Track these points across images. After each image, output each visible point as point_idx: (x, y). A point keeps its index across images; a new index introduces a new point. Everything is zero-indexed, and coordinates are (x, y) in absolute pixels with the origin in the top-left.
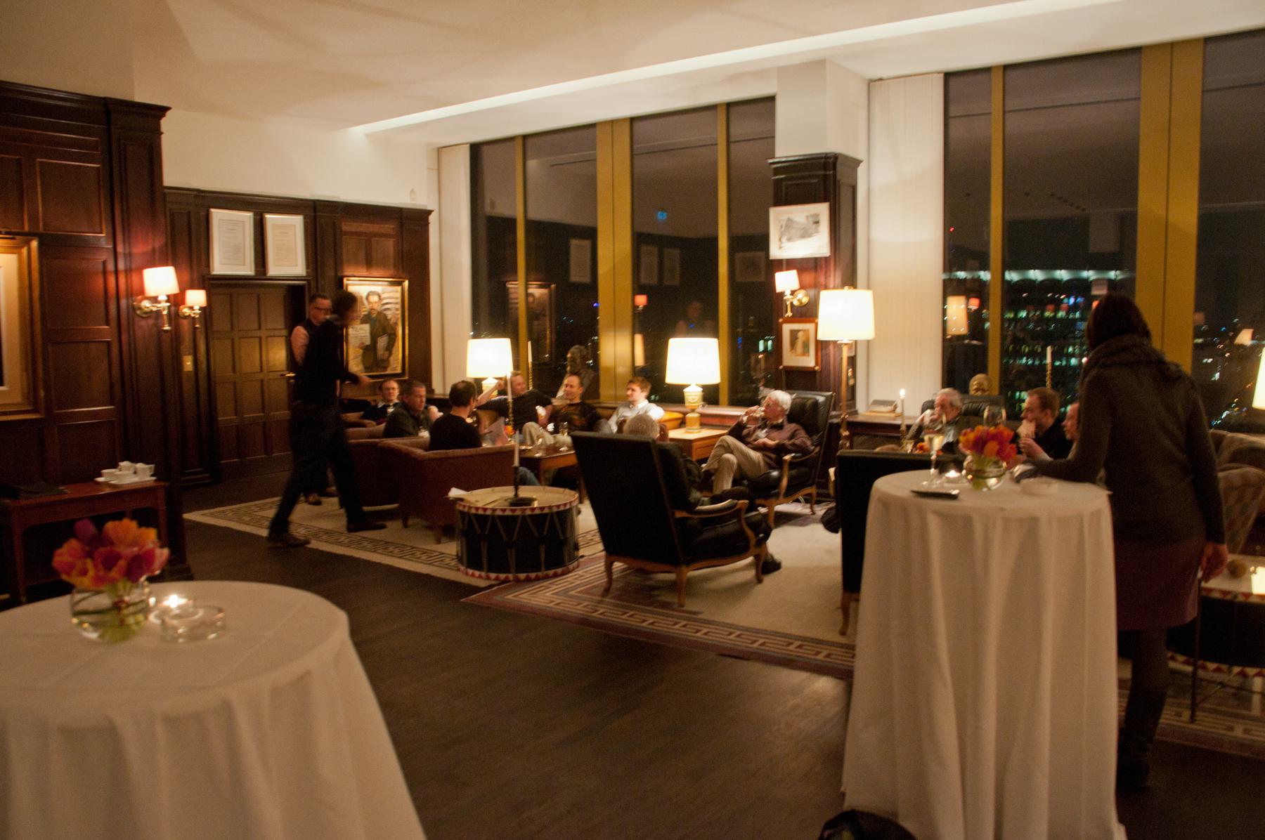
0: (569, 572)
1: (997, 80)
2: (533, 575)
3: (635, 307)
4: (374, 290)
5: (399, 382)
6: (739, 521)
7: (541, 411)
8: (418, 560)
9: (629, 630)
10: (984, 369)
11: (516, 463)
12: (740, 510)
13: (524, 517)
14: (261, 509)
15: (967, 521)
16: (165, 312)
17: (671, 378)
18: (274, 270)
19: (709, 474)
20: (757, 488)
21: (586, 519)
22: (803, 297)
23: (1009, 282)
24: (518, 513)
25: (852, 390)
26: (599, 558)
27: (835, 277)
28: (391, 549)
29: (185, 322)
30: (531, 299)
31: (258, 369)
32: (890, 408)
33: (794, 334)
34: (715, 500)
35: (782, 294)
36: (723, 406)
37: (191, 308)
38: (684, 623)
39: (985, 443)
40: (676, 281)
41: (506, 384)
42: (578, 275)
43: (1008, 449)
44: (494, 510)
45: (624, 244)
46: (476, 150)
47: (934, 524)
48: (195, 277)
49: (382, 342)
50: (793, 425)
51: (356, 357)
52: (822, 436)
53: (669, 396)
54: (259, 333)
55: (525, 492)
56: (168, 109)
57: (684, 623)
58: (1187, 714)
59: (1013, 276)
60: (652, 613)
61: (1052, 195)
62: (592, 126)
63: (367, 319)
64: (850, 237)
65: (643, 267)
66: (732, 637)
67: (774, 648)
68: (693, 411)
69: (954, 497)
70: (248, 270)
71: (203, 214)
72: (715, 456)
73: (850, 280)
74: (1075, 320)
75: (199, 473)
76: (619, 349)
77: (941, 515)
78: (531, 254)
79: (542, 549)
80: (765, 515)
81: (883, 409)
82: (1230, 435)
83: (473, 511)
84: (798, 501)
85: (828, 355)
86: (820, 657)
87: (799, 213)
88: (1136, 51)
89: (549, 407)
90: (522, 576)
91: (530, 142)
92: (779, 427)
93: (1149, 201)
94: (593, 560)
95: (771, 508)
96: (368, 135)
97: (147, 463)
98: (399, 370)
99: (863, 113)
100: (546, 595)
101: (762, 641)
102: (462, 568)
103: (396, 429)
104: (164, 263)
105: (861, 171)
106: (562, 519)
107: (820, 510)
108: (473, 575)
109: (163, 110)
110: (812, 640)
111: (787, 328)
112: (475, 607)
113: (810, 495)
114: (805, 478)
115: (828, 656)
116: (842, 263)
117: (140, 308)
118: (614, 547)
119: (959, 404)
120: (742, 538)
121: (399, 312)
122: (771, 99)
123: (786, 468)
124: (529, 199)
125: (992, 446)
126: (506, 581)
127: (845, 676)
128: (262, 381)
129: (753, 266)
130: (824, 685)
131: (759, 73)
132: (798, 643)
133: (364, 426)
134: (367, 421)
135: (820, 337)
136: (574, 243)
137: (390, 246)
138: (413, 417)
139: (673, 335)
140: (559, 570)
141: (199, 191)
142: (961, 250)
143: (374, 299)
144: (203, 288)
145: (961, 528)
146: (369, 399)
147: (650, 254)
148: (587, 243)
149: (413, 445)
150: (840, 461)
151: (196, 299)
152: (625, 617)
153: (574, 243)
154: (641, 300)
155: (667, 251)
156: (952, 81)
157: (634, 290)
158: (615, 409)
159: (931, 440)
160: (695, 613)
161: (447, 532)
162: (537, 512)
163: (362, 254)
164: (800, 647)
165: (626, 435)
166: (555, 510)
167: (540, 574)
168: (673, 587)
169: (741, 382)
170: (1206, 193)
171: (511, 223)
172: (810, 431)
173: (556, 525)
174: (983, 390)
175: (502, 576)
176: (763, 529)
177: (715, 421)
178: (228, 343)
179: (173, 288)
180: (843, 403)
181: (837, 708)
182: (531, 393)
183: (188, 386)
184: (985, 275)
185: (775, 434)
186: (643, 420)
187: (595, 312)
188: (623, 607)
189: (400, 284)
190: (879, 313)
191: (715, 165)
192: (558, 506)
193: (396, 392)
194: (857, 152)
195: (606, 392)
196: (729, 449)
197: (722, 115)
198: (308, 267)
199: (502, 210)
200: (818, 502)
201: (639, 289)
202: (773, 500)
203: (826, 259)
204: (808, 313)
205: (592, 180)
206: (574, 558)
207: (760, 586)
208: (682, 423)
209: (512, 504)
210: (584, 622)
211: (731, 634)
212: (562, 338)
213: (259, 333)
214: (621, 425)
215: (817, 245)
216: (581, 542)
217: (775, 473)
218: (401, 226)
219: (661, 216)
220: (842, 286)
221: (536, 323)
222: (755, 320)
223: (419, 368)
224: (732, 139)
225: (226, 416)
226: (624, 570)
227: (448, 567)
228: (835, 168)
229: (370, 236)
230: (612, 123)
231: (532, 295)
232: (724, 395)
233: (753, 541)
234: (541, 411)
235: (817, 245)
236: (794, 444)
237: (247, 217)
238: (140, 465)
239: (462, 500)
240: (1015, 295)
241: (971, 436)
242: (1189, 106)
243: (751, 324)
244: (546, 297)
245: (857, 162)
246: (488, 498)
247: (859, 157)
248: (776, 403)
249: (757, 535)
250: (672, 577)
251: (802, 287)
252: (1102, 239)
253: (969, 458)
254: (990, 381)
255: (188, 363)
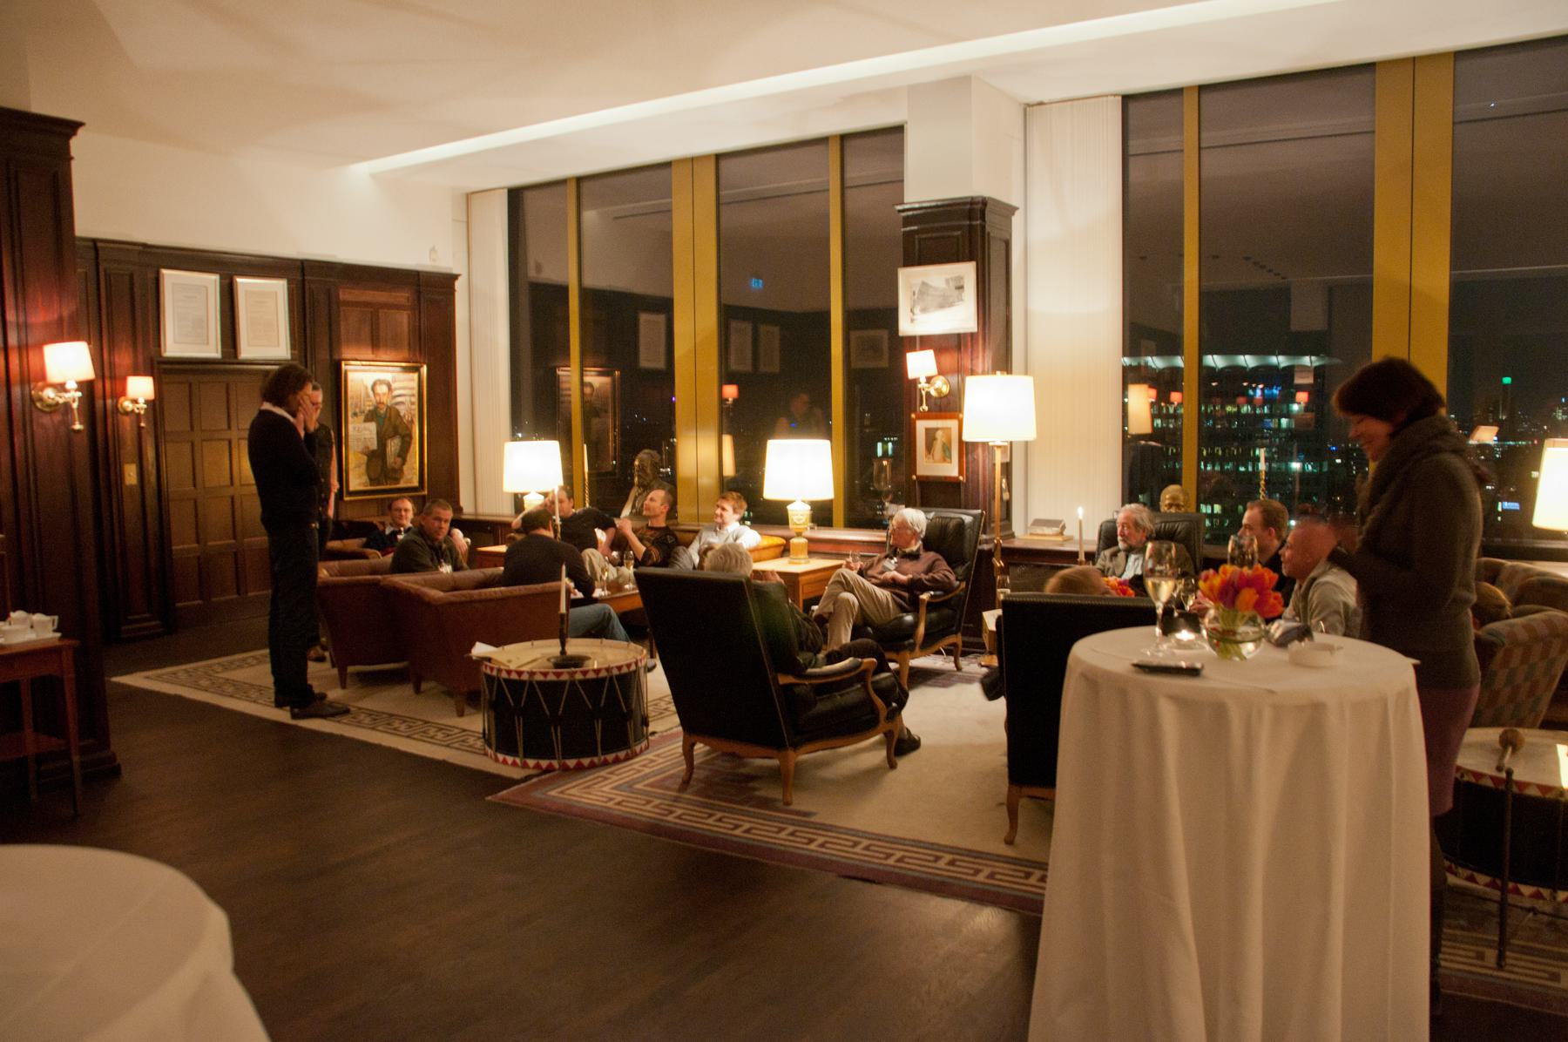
0: (635, 755)
1: (1190, 103)
2: (586, 761)
3: (722, 400)
4: (377, 379)
5: (413, 499)
6: (865, 687)
7: (601, 535)
8: (431, 740)
9: (715, 841)
10: (1175, 479)
11: (563, 609)
12: (865, 671)
13: (573, 683)
14: (226, 669)
15: (1219, 711)
16: (75, 405)
17: (771, 492)
18: (247, 351)
19: (822, 620)
20: (882, 637)
21: (657, 683)
22: (941, 386)
23: (1212, 369)
24: (565, 677)
25: (1007, 506)
26: (676, 735)
27: (984, 358)
28: (396, 724)
29: (127, 420)
30: (587, 390)
31: (228, 482)
32: (1056, 530)
33: (931, 434)
34: (833, 658)
35: (915, 382)
36: (838, 528)
37: (135, 401)
38: (791, 829)
39: (1237, 592)
40: (775, 368)
41: (553, 503)
42: (649, 359)
43: (1272, 600)
44: (532, 674)
45: (709, 319)
46: (516, 196)
47: (1169, 715)
48: (141, 358)
49: (393, 446)
50: (932, 554)
51: (358, 466)
52: (969, 569)
53: (768, 515)
54: (227, 435)
55: (576, 647)
56: (80, 124)
57: (791, 829)
58: (1491, 954)
59: (1215, 361)
60: (748, 814)
61: (1247, 259)
62: (667, 165)
63: (372, 416)
64: (1002, 308)
65: (732, 348)
66: (858, 849)
67: (917, 865)
68: (799, 535)
69: (1193, 672)
70: (212, 350)
71: (151, 276)
72: (829, 596)
73: (1004, 363)
74: (1263, 416)
75: (145, 620)
76: (702, 453)
77: (1180, 701)
78: (590, 332)
79: (599, 726)
80: (897, 673)
81: (1047, 531)
82: (1508, 563)
83: (504, 675)
84: (939, 653)
85: (975, 461)
86: (981, 878)
87: (937, 276)
88: (1369, 67)
89: (612, 530)
90: (571, 763)
91: (585, 185)
92: (914, 556)
93: (1387, 261)
94: (667, 738)
95: (903, 663)
96: (374, 177)
97: (46, 613)
98: (416, 483)
99: (1018, 148)
100: (604, 790)
101: (899, 854)
102: (489, 751)
103: (406, 563)
104: (74, 336)
105: (1017, 220)
106: (626, 683)
107: (975, 666)
108: (505, 762)
109: (72, 127)
110: (971, 853)
111: (921, 426)
112: (506, 809)
113: (955, 645)
114: (952, 623)
115: (991, 876)
116: (993, 340)
117: (41, 400)
118: (694, 724)
119: (1149, 525)
120: (868, 709)
121: (416, 407)
122: (899, 130)
123: (923, 610)
124: (584, 261)
125: (1249, 596)
126: (550, 769)
127: (1029, 917)
128: (233, 498)
129: (873, 347)
130: (988, 920)
131: (884, 94)
132: (948, 857)
133: (365, 557)
134: (369, 551)
135: (966, 438)
136: (644, 317)
137: (403, 319)
138: (431, 547)
139: (772, 434)
140: (622, 754)
141: (145, 245)
142: (1146, 329)
143: (382, 389)
144: (151, 375)
145: (1209, 720)
146: (375, 520)
147: (742, 332)
148: (661, 318)
149: (427, 584)
150: (1032, 628)
151: (140, 389)
152: (710, 821)
153: (644, 317)
154: (731, 391)
155: (763, 329)
156: (1132, 106)
157: (720, 378)
158: (696, 532)
159: (1156, 587)
160: (806, 814)
161: (471, 700)
162: (591, 675)
163: (366, 330)
164: (952, 863)
165: (707, 573)
166: (615, 672)
167: (596, 760)
168: (777, 776)
169: (861, 500)
170: (1460, 255)
171: (561, 291)
172: (952, 563)
173: (626, 683)
174: (1178, 506)
175: (544, 763)
176: (896, 697)
177: (827, 548)
178: (187, 447)
179: (87, 371)
180: (997, 524)
181: (1005, 958)
182: (586, 512)
183: (130, 507)
184: (1179, 362)
185: (908, 565)
186: (730, 554)
187: (671, 407)
188: (705, 806)
189: (417, 370)
190: (1042, 410)
191: (825, 219)
192: (619, 668)
193: (410, 515)
194: (1009, 194)
195: (684, 510)
196: (847, 586)
197: (834, 149)
198: (293, 347)
199: (550, 275)
200: (964, 654)
201: (727, 377)
202: (907, 654)
203: (972, 334)
204: (949, 406)
205: (666, 239)
206: (641, 736)
207: (892, 774)
208: (785, 551)
209: (557, 666)
210: (656, 829)
211: (856, 844)
212: (628, 444)
213: (227, 435)
214: (703, 554)
215: (961, 317)
216: (651, 711)
217: (909, 618)
218: (419, 293)
219: (756, 284)
220: (994, 371)
221: (595, 421)
222: (880, 413)
223: (442, 480)
224: (848, 183)
225: (183, 545)
226: (708, 753)
227: (472, 750)
228: (983, 217)
229: (375, 308)
230: (693, 160)
231: (591, 385)
232: (839, 514)
233: (883, 712)
234: (601, 535)
235: (961, 317)
236: (934, 580)
237: (212, 281)
238: (38, 617)
239: (489, 660)
240: (1229, 384)
241: (1217, 581)
242: (1436, 138)
243: (867, 423)
244: (609, 387)
245: (1013, 210)
246: (525, 657)
247: (1014, 203)
248: (903, 525)
249: (888, 705)
250: (775, 762)
251: (941, 372)
252: (1307, 315)
253: (1212, 612)
254: (1186, 494)
255: (131, 475)
